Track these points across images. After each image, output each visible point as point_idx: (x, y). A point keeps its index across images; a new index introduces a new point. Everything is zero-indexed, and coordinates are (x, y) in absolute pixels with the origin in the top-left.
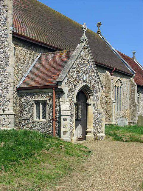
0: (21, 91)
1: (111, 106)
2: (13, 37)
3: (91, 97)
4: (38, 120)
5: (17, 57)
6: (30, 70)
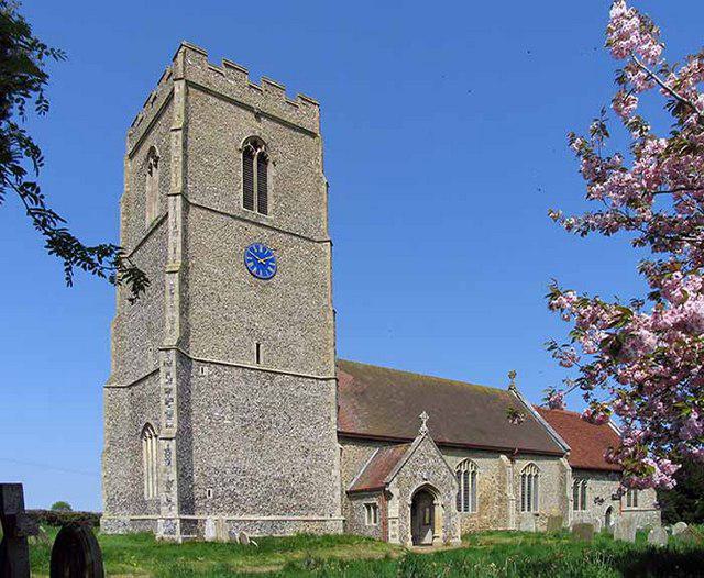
0: (352, 495)
2: (338, 437)
4: (368, 522)
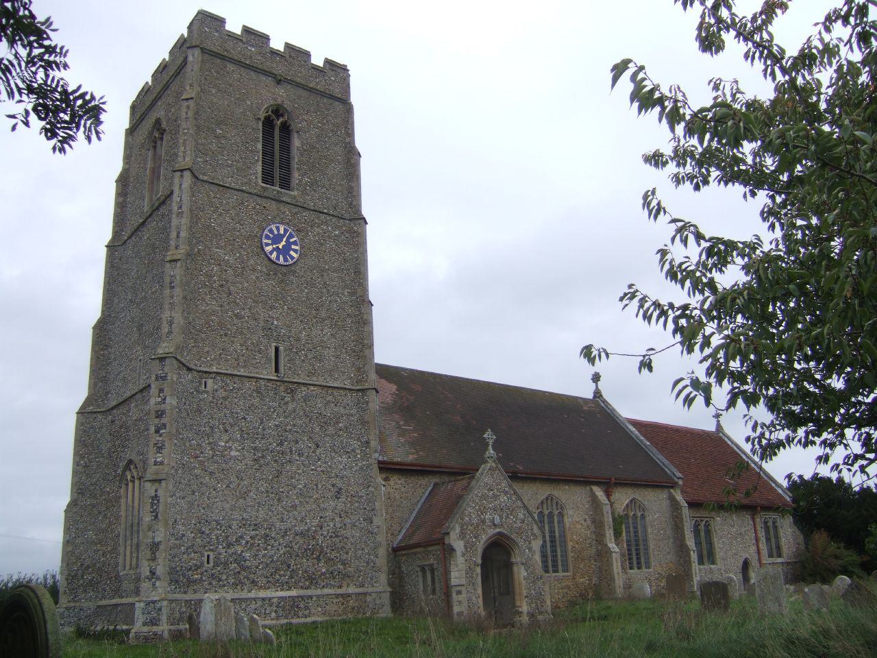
1: (610, 560)
3: (517, 551)
5: (389, 498)
6: (414, 515)
